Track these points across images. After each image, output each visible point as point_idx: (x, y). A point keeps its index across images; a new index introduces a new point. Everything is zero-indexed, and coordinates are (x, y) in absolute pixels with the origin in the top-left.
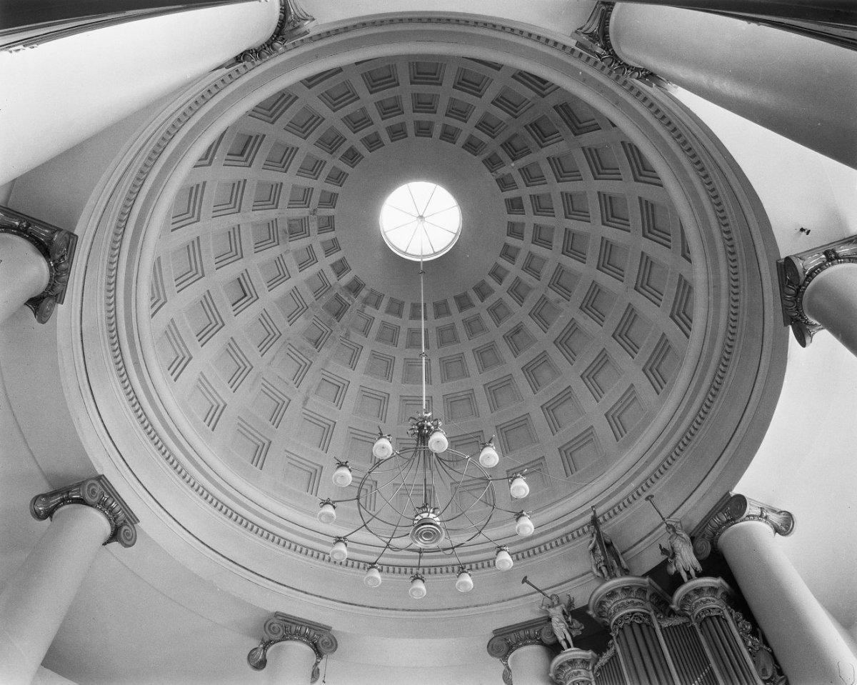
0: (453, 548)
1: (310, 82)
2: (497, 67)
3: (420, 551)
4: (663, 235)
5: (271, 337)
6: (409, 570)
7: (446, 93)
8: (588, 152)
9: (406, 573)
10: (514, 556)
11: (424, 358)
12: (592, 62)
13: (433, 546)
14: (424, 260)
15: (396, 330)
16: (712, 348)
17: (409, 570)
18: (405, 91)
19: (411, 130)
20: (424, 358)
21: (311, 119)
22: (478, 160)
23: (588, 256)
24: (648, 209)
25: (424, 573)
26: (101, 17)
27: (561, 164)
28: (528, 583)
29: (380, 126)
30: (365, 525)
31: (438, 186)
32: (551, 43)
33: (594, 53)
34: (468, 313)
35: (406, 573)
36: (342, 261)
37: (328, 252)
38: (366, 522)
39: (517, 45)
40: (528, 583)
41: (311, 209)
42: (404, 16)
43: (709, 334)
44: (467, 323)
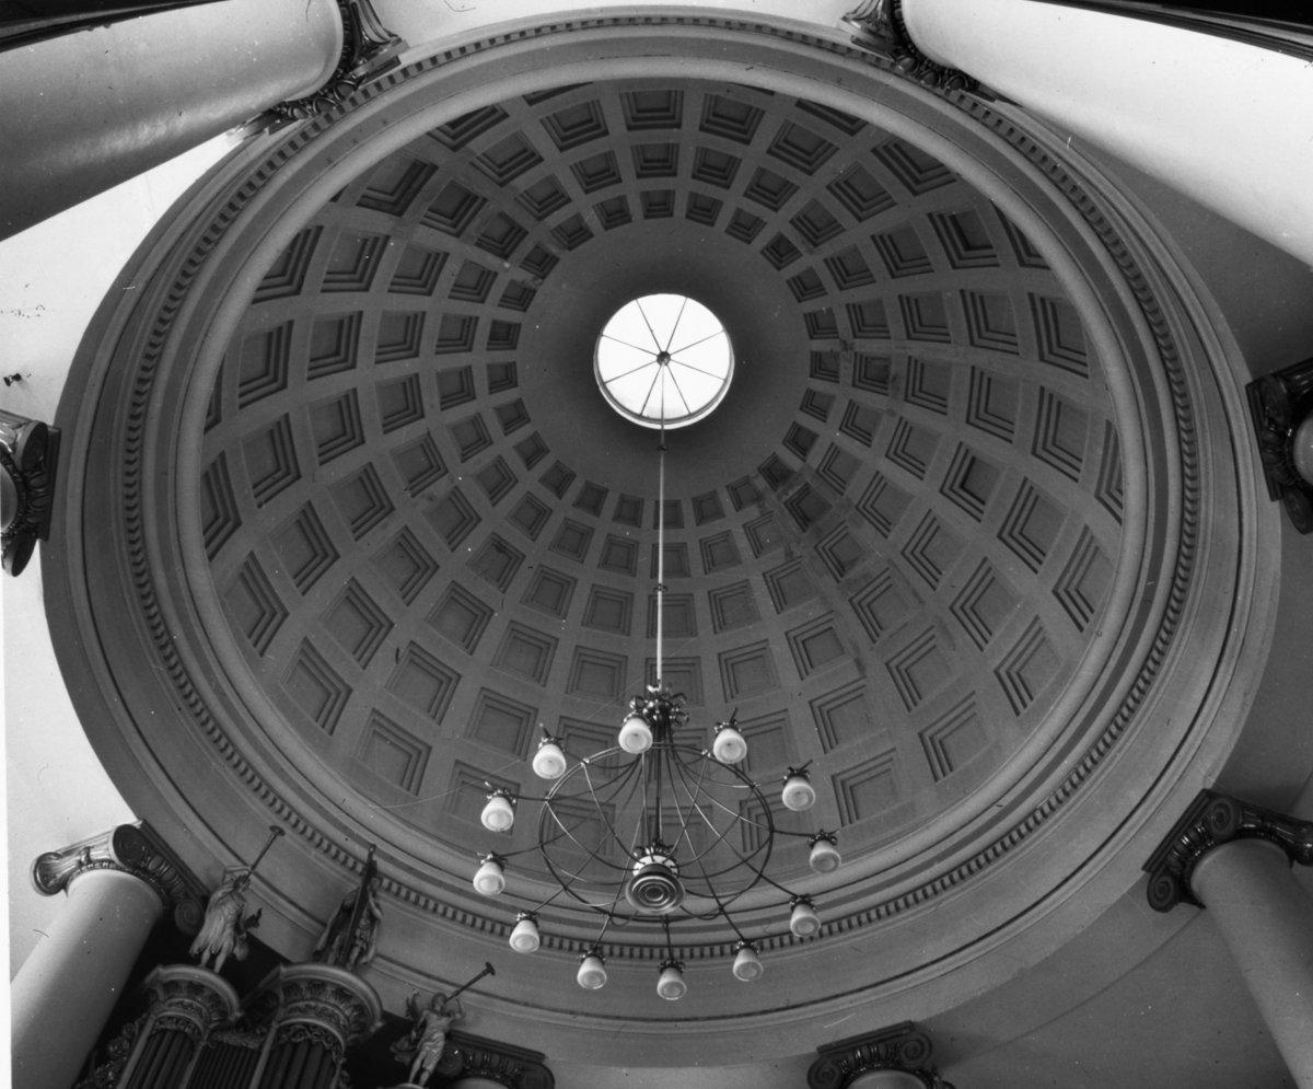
0: (612, 915)
1: (533, 99)
2: (852, 125)
3: (667, 919)
4: (1069, 459)
5: (919, 549)
6: (657, 952)
7: (753, 156)
8: (969, 299)
9: (651, 957)
10: (546, 940)
11: (660, 593)
12: (373, 91)
13: (645, 911)
14: (667, 427)
15: (585, 535)
16: (171, 578)
17: (657, 952)
18: (689, 138)
19: (681, 206)
20: (660, 593)
21: (520, 154)
22: (566, 258)
23: (929, 469)
24: (1052, 408)
25: (682, 956)
26: (1202, 14)
27: (1056, 321)
28: (484, 974)
29: (632, 189)
30: (761, 876)
31: (640, 300)
32: (428, 65)
33: (368, 76)
34: (584, 518)
35: (651, 957)
36: (518, 404)
37: (495, 386)
38: (750, 862)
39: (489, 65)
40: (484, 974)
41: (850, 340)
42: (796, 29)
43: (177, 558)
44: (707, 547)
